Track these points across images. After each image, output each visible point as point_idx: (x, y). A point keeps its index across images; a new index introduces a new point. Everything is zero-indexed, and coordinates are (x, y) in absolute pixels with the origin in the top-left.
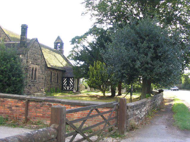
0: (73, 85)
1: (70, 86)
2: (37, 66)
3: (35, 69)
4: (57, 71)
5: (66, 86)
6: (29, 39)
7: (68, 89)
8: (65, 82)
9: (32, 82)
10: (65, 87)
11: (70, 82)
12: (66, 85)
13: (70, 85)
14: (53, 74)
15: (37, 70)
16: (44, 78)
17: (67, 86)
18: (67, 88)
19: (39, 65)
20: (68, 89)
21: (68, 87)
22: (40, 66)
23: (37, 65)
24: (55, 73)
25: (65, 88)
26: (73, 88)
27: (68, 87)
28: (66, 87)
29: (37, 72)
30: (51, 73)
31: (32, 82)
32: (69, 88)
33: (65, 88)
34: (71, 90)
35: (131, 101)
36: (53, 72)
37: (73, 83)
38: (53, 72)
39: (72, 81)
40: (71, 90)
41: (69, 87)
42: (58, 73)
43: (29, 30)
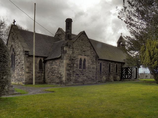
0: (131, 74)
1: (129, 75)
2: (86, 57)
3: (83, 60)
4: (115, 63)
5: (125, 75)
6: (74, 35)
7: (127, 77)
8: (124, 72)
9: (79, 71)
10: (124, 76)
11: (129, 71)
12: (125, 74)
13: (129, 74)
14: (111, 66)
15: (87, 61)
16: (95, 67)
17: (126, 75)
18: (125, 77)
19: (88, 56)
20: (127, 77)
21: (127, 76)
22: (89, 57)
23: (85, 56)
24: (114, 65)
25: (124, 77)
26: (131, 76)
27: (127, 76)
28: (125, 76)
29: (87, 63)
30: (101, 65)
31: (79, 71)
32: (128, 77)
33: (124, 77)
34: (129, 78)
35: (68, 74)
36: (112, 64)
37: (131, 72)
38: (112, 64)
39: (130, 71)
40: (129, 78)
41: (128, 76)
42: (117, 65)
43: (74, 24)
